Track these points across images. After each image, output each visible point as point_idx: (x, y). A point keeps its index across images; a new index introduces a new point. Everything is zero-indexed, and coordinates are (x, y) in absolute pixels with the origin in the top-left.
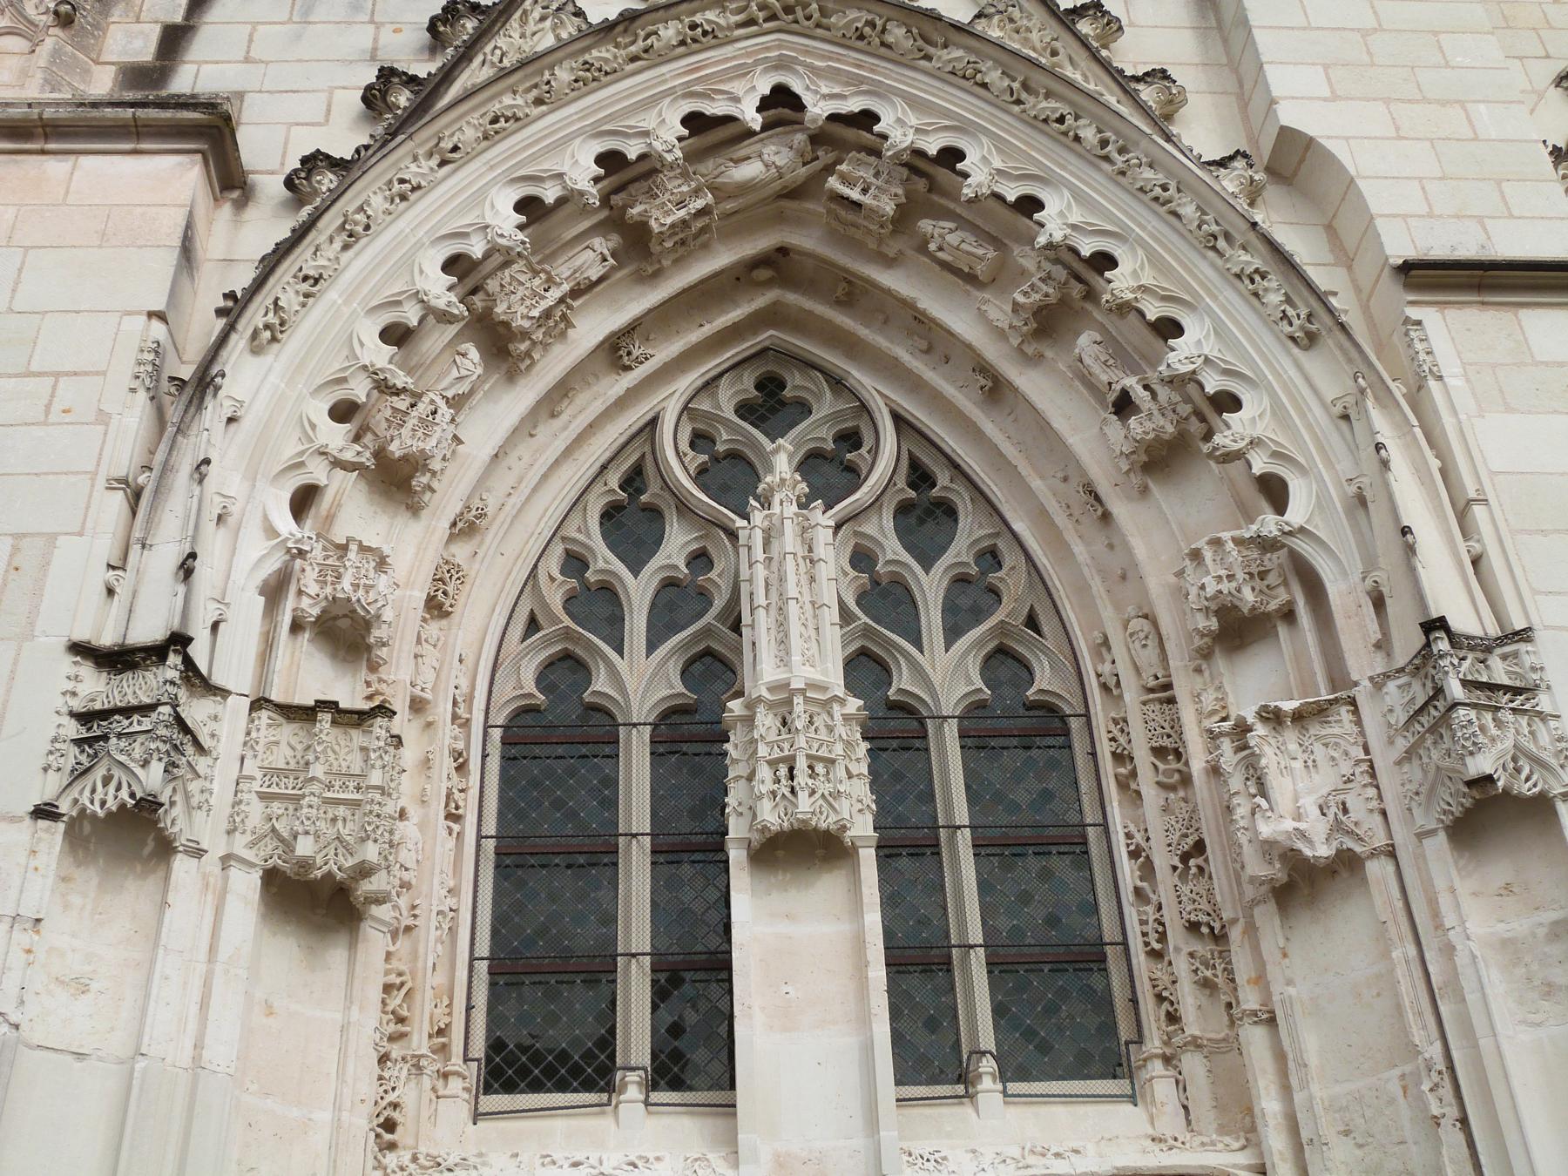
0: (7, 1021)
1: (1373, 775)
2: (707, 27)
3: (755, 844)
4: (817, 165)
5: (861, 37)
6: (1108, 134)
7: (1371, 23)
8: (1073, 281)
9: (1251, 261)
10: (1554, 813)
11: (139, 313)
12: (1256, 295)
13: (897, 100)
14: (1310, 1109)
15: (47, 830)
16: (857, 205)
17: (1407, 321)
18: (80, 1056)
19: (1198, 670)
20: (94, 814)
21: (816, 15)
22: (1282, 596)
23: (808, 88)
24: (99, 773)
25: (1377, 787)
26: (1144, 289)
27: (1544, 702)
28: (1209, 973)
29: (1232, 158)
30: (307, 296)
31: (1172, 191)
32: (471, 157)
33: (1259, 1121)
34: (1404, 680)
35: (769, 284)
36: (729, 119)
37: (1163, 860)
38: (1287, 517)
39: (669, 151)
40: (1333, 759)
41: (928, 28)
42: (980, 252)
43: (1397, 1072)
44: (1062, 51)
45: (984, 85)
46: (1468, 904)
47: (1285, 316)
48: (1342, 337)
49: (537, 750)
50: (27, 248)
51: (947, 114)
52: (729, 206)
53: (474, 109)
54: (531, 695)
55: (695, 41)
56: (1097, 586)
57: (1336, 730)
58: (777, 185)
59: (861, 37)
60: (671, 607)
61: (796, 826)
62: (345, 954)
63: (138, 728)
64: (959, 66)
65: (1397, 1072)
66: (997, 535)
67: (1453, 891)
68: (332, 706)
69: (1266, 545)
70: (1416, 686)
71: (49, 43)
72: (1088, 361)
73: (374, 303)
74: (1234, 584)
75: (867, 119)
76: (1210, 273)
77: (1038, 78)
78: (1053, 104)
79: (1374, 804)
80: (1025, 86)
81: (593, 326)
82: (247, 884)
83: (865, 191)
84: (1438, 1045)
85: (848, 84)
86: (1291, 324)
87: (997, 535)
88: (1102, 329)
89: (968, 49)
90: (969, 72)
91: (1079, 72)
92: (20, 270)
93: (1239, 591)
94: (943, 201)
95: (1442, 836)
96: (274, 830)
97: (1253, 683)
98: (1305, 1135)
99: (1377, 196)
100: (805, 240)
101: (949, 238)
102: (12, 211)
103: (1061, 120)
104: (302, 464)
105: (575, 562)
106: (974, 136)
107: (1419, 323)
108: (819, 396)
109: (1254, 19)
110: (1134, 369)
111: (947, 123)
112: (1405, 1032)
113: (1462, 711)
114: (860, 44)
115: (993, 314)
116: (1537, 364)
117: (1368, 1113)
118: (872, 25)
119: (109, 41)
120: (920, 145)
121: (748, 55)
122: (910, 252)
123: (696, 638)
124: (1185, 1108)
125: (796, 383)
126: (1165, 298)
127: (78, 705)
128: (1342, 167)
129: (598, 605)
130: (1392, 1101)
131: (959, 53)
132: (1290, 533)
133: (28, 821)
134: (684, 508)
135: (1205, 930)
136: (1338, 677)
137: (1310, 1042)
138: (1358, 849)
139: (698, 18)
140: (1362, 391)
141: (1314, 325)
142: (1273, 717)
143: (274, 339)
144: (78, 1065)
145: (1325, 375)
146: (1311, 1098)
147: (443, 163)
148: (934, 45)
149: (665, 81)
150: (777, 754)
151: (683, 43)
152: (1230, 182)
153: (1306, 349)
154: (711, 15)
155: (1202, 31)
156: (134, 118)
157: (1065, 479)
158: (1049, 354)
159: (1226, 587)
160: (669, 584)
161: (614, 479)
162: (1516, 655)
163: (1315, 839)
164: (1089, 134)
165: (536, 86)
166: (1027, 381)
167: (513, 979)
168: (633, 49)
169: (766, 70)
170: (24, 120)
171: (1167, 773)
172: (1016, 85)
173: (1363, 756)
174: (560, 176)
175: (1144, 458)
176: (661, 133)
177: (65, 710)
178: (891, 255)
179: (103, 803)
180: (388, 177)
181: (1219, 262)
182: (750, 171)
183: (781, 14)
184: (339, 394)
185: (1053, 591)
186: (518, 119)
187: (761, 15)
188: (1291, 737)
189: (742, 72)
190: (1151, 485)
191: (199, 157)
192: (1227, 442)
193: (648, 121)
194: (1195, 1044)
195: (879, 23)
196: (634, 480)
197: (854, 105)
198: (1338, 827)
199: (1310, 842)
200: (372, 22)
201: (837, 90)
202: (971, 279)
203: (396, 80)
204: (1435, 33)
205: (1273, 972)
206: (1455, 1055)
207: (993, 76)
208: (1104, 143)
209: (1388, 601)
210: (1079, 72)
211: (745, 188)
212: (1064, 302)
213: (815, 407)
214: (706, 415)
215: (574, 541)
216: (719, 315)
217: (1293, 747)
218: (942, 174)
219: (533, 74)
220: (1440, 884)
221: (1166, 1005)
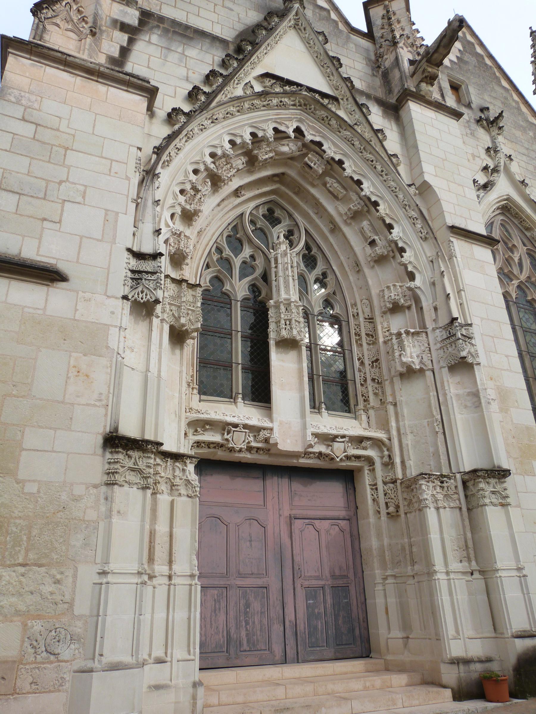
1: (430, 350)
4: (302, 153)
5: (323, 120)
6: (384, 169)
7: (444, 158)
10: (473, 367)
11: (135, 147)
12: (414, 224)
13: (329, 141)
14: (404, 426)
16: (310, 167)
17: (450, 241)
18: (133, 369)
19: (382, 316)
21: (313, 109)
22: (409, 303)
24: (140, 289)
27: (473, 341)
28: (377, 391)
32: (219, 123)
33: (390, 428)
34: (441, 330)
36: (284, 132)
37: (367, 362)
38: (415, 283)
42: (342, 191)
43: (427, 420)
44: (373, 141)
45: (353, 145)
46: (451, 386)
49: (209, 302)
51: (342, 150)
52: (277, 157)
54: (209, 286)
55: (280, 106)
56: (355, 289)
57: (421, 339)
58: (290, 156)
59: (323, 120)
63: (150, 278)
64: (348, 137)
65: (427, 420)
66: (327, 269)
67: (448, 381)
68: (186, 281)
69: (410, 289)
70: (444, 332)
72: (365, 229)
75: (320, 144)
76: (402, 214)
77: (368, 147)
78: (371, 156)
79: (430, 358)
80: (364, 148)
81: (236, 183)
82: (166, 328)
83: (315, 164)
84: (440, 415)
85: (317, 132)
86: (422, 233)
87: (327, 269)
88: (370, 221)
90: (350, 140)
91: (378, 148)
92: (95, 121)
94: (333, 173)
95: (447, 368)
96: (173, 314)
97: (397, 323)
98: (402, 432)
99: (446, 207)
100: (292, 173)
103: (372, 161)
104: (174, 206)
105: (219, 250)
106: (348, 158)
107: (452, 242)
108: (285, 218)
109: (420, 147)
110: (377, 234)
112: (431, 412)
113: (461, 341)
114: (322, 122)
116: (475, 259)
119: (103, 45)
120: (334, 157)
121: (292, 114)
122: (320, 185)
123: (253, 280)
125: (278, 213)
126: (391, 218)
130: (424, 427)
131: (349, 133)
132: (416, 288)
133: (121, 299)
134: (250, 241)
135: (376, 381)
137: (405, 411)
138: (425, 368)
139: (283, 100)
140: (439, 256)
141: (428, 235)
142: (407, 333)
143: (168, 166)
145: (428, 250)
146: (405, 424)
147: (212, 122)
150: (286, 318)
152: (412, 190)
153: (424, 241)
154: (286, 100)
158: (353, 224)
159: (397, 297)
160: (244, 262)
161: (230, 227)
162: (468, 329)
164: (379, 168)
165: (238, 106)
166: (346, 230)
168: (265, 103)
170: (93, 69)
172: (362, 148)
176: (268, 131)
179: (142, 299)
183: (303, 105)
184: (182, 187)
186: (232, 115)
187: (298, 104)
188: (410, 337)
189: (290, 119)
190: (376, 266)
191: (147, 99)
192: (404, 261)
193: (264, 126)
194: (373, 408)
195: (329, 117)
197: (317, 139)
198: (421, 362)
199: (415, 364)
201: (314, 133)
202: (336, 197)
203: (200, 91)
204: (458, 165)
205: (397, 393)
206: (444, 418)
207: (357, 143)
208: (382, 171)
209: (438, 310)
210: (378, 148)
211: (283, 153)
212: (362, 210)
214: (255, 216)
215: (220, 244)
216: (264, 187)
217: (411, 341)
218: (336, 166)
220: (445, 379)
221: (364, 397)
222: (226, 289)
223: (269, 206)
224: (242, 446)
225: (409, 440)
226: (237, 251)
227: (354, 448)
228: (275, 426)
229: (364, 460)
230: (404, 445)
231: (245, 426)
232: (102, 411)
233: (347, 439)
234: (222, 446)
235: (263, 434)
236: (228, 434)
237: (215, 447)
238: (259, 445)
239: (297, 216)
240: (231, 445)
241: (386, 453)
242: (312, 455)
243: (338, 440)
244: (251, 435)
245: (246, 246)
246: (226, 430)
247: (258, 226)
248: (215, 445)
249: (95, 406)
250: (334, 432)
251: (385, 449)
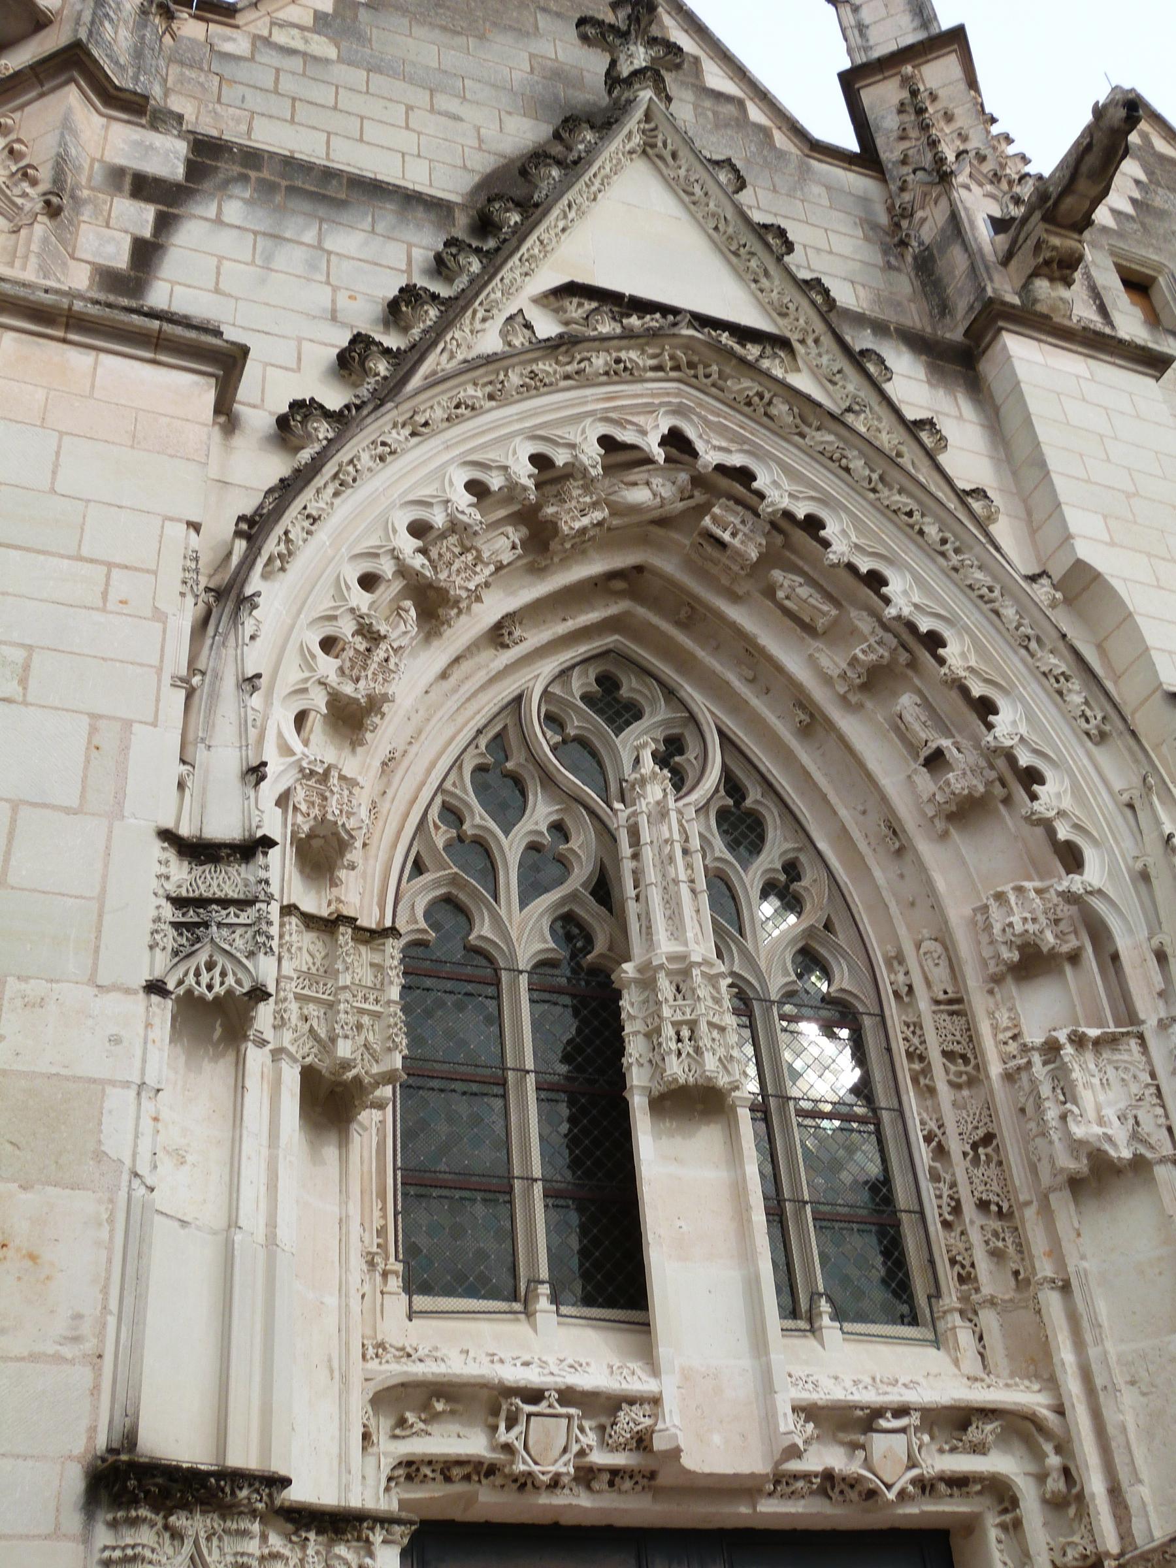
0: (144, 1183)
1: (1159, 1094)
2: (629, 365)
3: (655, 1093)
5: (749, 404)
7: (1132, 489)
8: (901, 649)
9: (1057, 663)
11: (179, 520)
12: (1060, 693)
13: (772, 464)
15: (158, 1005)
16: (722, 545)
18: (184, 1223)
19: (991, 992)
20: (202, 998)
21: (715, 376)
22: (1071, 943)
23: (700, 436)
24: (202, 958)
25: (1163, 1107)
26: (971, 669)
28: (1000, 1244)
29: (1040, 575)
30: (309, 533)
31: (997, 593)
32: (435, 433)
33: (1058, 1370)
35: (620, 594)
37: (956, 1147)
39: (594, 467)
40: (1123, 1080)
41: (808, 411)
42: (825, 608)
44: (907, 455)
45: (847, 470)
47: (1083, 715)
48: (1131, 742)
49: (429, 982)
50: (62, 434)
51: (813, 486)
52: (616, 522)
53: (443, 392)
56: (894, 909)
57: (1126, 1057)
58: (656, 514)
59: (749, 404)
60: (535, 868)
61: (701, 1081)
62: (337, 1152)
66: (800, 850)
69: (1070, 897)
71: (38, 229)
72: (908, 718)
73: (357, 550)
74: (1037, 927)
77: (894, 475)
78: (904, 499)
79: (1162, 1120)
80: (881, 478)
81: (494, 607)
82: (291, 1078)
83: (734, 535)
85: (732, 441)
86: (1087, 721)
87: (800, 850)
89: (837, 435)
90: (836, 456)
91: (925, 475)
92: (58, 453)
93: (1041, 932)
94: (793, 557)
96: (311, 1030)
97: (1041, 1012)
98: (1099, 1382)
100: (667, 565)
101: (799, 590)
102: (40, 394)
103: (910, 514)
105: (452, 814)
106: (833, 509)
108: (653, 702)
110: (948, 734)
111: (813, 494)
114: (747, 409)
115: (824, 662)
117: (1152, 1368)
118: (761, 396)
119: (82, 240)
121: (653, 395)
122: (757, 595)
123: (564, 900)
124: (981, 1354)
125: (630, 687)
127: (171, 888)
128: (1122, 603)
129: (479, 853)
131: (831, 438)
132: (1091, 893)
133: (141, 995)
134: (548, 780)
135: (994, 1208)
136: (1132, 1018)
138: (1149, 1155)
139: (623, 355)
143: (283, 569)
144: (182, 1232)
145: (1113, 771)
146: (1105, 1353)
147: (413, 434)
148: (810, 426)
149: (586, 403)
150: (679, 1017)
151: (607, 373)
152: (1042, 592)
153: (1096, 744)
154: (633, 355)
155: (996, 462)
156: (160, 331)
157: (864, 812)
158: (869, 705)
159: (1031, 927)
160: (534, 847)
161: (483, 742)
163: (1119, 1143)
164: (932, 531)
165: (491, 383)
166: (848, 724)
167: (422, 1191)
168: (569, 368)
169: (666, 413)
171: (959, 1074)
172: (875, 476)
173: (1149, 1080)
174: (505, 468)
175: (954, 808)
176: (584, 446)
177: (161, 892)
178: (740, 593)
179: (210, 987)
180: (373, 437)
181: (1029, 659)
182: (639, 495)
185: (852, 906)
186: (473, 409)
187: (669, 364)
190: (952, 830)
191: (213, 381)
192: (1042, 809)
193: (571, 434)
194: (992, 1302)
195: (767, 396)
196: (499, 743)
197: (736, 460)
198: (1135, 1136)
200: (328, 283)
201: (724, 444)
202: (808, 628)
203: (374, 348)
205: (1068, 1247)
207: (857, 464)
208: (944, 541)
209: (1171, 960)
210: (925, 475)
211: (635, 509)
213: (647, 710)
214: (560, 700)
217: (1092, 1066)
219: (491, 372)
221: (957, 1268)
224: (559, 1468)
225: (1126, 1411)
227: (941, 1451)
228: (668, 1387)
229: (980, 1493)
230: (1111, 1430)
231: (568, 1396)
232: (82, 1375)
233: (914, 1419)
234: (491, 1470)
235: (630, 1420)
236: (509, 1428)
237: (467, 1478)
238: (619, 1459)
240: (522, 1467)
241: (1054, 1461)
242: (800, 1484)
243: (883, 1423)
244: (587, 1424)
246: (503, 1414)
247: (571, 732)
248: (467, 1469)
249: (58, 1359)
250: (870, 1397)
251: (1048, 1448)
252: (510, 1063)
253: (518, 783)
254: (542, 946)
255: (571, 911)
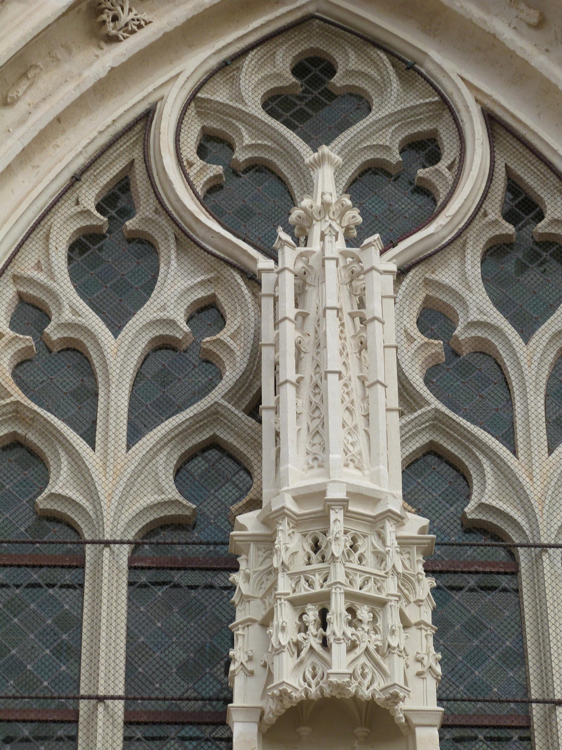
3: (270, 717)
54: (175, 502)
61: (327, 692)
108: (382, 87)
125: (350, 67)
134: (187, 239)
150: (304, 590)
160: (163, 346)
161: (89, 196)
213: (376, 102)
214: (223, 110)
215: (31, 281)
222: (482, 507)
223: (305, 46)
226: (117, 299)
239: (446, 65)
245: (168, 264)
247: (241, 156)
252: (534, 694)
253: (144, 245)
254: (157, 498)
255: (214, 436)
